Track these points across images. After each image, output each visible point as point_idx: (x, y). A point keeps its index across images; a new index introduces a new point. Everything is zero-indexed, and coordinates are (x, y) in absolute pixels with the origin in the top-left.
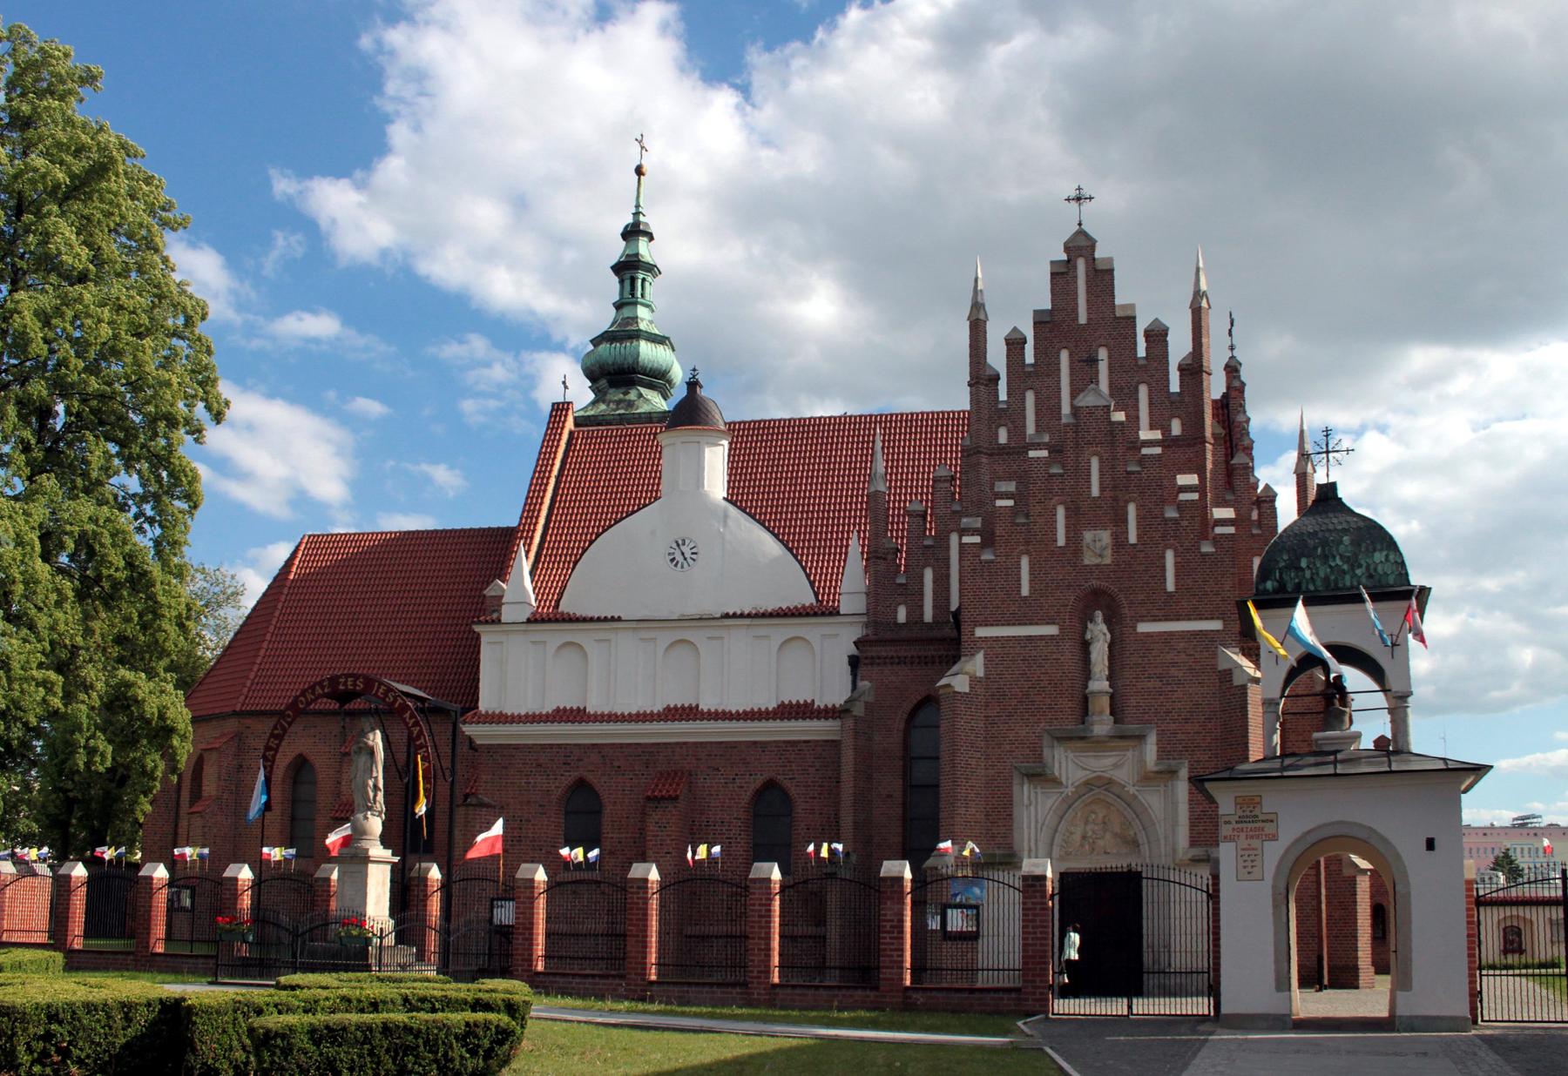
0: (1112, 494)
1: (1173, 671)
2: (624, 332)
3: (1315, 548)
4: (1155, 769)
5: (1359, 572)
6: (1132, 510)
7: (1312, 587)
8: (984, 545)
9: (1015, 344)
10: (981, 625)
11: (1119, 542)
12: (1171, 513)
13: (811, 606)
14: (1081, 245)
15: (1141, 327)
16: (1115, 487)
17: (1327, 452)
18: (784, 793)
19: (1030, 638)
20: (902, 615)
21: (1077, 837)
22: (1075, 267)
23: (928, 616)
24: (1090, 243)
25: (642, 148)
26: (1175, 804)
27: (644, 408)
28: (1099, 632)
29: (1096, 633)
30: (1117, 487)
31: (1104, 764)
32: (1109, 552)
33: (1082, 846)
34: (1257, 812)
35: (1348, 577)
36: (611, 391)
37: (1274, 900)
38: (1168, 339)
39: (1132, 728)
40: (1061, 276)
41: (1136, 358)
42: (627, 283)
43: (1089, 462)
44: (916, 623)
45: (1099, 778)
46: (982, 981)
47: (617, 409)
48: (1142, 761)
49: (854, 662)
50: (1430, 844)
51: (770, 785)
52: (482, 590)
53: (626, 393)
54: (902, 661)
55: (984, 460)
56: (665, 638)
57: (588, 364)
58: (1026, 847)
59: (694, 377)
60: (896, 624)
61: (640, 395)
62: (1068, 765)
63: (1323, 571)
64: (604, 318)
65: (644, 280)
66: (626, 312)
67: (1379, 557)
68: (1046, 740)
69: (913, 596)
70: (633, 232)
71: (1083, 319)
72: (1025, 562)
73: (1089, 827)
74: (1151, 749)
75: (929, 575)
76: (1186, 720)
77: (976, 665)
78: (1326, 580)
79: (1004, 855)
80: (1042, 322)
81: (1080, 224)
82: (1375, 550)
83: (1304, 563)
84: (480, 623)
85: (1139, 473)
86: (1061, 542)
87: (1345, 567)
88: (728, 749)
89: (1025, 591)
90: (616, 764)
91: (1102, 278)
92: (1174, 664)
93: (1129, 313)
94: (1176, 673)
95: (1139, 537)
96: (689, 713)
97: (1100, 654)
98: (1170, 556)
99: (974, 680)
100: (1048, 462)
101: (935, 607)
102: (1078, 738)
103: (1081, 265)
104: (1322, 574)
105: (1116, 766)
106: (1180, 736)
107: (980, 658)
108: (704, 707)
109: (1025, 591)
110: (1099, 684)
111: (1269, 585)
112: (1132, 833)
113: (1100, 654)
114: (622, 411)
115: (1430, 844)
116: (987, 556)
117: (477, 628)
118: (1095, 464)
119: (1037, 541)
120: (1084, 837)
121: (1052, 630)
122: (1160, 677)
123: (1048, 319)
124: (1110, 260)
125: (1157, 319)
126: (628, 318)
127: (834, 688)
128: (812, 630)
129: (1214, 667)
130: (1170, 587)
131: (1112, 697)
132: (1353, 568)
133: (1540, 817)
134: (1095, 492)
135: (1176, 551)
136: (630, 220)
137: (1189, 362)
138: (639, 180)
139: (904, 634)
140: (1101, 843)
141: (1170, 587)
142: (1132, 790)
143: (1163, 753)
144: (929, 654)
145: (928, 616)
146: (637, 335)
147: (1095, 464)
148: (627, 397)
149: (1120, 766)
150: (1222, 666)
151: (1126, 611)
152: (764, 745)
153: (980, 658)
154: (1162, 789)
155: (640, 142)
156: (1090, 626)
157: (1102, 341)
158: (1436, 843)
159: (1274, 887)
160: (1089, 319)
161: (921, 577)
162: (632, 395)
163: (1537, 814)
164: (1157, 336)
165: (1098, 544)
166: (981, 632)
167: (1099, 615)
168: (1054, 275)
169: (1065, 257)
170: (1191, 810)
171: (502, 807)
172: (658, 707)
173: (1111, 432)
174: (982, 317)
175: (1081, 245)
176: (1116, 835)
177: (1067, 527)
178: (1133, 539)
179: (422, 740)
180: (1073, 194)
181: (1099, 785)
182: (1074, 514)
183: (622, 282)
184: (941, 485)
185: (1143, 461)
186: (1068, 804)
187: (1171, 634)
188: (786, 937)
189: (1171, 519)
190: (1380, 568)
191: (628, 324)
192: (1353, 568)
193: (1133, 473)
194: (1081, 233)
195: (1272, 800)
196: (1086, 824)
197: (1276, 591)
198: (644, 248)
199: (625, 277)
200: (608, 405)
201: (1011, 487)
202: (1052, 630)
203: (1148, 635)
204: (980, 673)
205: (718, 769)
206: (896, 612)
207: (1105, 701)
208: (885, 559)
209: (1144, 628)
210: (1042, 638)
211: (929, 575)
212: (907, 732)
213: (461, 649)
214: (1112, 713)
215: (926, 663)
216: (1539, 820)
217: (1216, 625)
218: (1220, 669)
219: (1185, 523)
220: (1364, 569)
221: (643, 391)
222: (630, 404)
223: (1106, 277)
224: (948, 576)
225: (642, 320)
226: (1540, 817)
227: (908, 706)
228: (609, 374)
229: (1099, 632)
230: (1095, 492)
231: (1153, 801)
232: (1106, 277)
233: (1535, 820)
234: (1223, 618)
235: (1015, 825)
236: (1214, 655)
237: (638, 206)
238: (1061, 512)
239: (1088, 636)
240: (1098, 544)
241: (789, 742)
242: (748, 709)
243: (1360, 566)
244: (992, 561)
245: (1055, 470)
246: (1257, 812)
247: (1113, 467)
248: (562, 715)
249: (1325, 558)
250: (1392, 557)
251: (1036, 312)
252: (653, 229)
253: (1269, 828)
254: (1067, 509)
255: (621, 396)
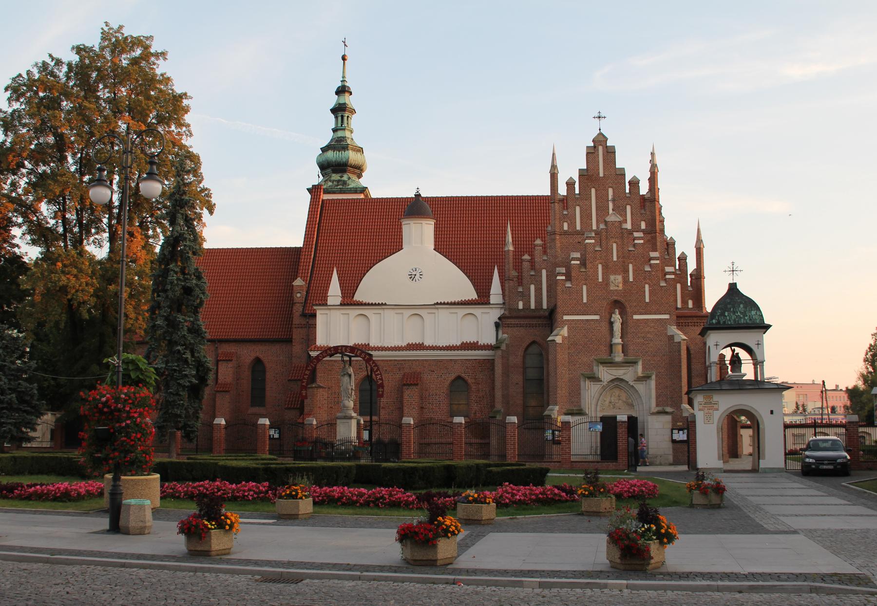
0: (622, 260)
1: (649, 335)
2: (338, 144)
3: (730, 309)
4: (642, 375)
5: (746, 318)
6: (631, 266)
7: (729, 323)
8: (566, 280)
9: (570, 184)
10: (566, 315)
11: (625, 280)
12: (647, 269)
13: (477, 300)
14: (600, 140)
15: (628, 178)
16: (624, 257)
17: (733, 271)
18: (465, 381)
19: (587, 320)
20: (521, 305)
21: (607, 402)
22: (598, 150)
23: (533, 306)
24: (605, 139)
25: (345, 45)
26: (650, 389)
27: (352, 185)
28: (617, 318)
29: (616, 318)
30: (625, 257)
31: (619, 373)
32: (621, 285)
33: (609, 406)
34: (711, 401)
35: (742, 320)
36: (334, 175)
37: (717, 430)
38: (640, 185)
39: (631, 358)
40: (591, 153)
41: (626, 193)
42: (340, 118)
43: (612, 246)
44: (527, 309)
45: (617, 378)
46: (573, 459)
47: (338, 185)
48: (636, 372)
49: (497, 325)
50: (772, 412)
51: (459, 378)
52: (291, 283)
53: (341, 177)
54: (521, 326)
55: (558, 237)
56: (408, 313)
57: (321, 160)
58: (587, 407)
59: (418, 192)
60: (518, 309)
61: (349, 178)
62: (606, 374)
63: (734, 317)
64: (327, 137)
65: (348, 117)
66: (340, 134)
67: (753, 313)
68: (595, 363)
69: (526, 297)
70: (342, 90)
71: (601, 175)
72: (585, 287)
73: (612, 398)
74: (640, 367)
75: (532, 287)
76: (654, 356)
77: (565, 331)
78: (735, 320)
79: (577, 410)
80: (582, 174)
81: (600, 130)
82: (752, 310)
83: (726, 314)
84: (317, 305)
85: (634, 251)
86: (600, 280)
87: (742, 316)
88: (438, 362)
89: (585, 301)
90: (385, 369)
91: (610, 153)
92: (649, 332)
93: (622, 172)
94: (650, 336)
95: (634, 279)
96: (420, 347)
97: (617, 327)
98: (647, 286)
99: (564, 338)
100: (594, 245)
101: (535, 302)
102: (609, 363)
103: (600, 148)
104: (733, 318)
105: (624, 374)
106: (652, 362)
107: (566, 328)
108: (427, 344)
109: (585, 301)
110: (617, 340)
111: (714, 321)
112: (630, 401)
113: (617, 327)
114: (341, 187)
115: (772, 412)
116: (568, 285)
117: (315, 308)
118: (615, 245)
119: (590, 280)
120: (610, 402)
121: (597, 317)
122: (643, 338)
123: (586, 174)
124: (613, 147)
125: (614, 146)
126: (341, 137)
127: (488, 337)
128: (478, 311)
129: (666, 334)
130: (647, 300)
131: (623, 346)
132: (744, 316)
133: (778, 378)
134: (615, 259)
135: (649, 285)
136: (340, 84)
137: (695, 273)
138: (344, 63)
139: (522, 313)
140: (618, 405)
141: (647, 300)
142: (632, 384)
143: (644, 368)
144: (534, 323)
145: (533, 306)
146: (345, 148)
147: (615, 245)
148: (343, 179)
149: (627, 374)
150: (669, 334)
151: (628, 310)
152: (456, 361)
153: (566, 328)
154: (644, 382)
155: (344, 42)
156: (613, 315)
157: (610, 185)
158: (774, 412)
159: (718, 426)
160: (604, 175)
161: (529, 289)
162: (345, 178)
163: (776, 376)
164: (635, 183)
165: (617, 281)
166: (566, 317)
167: (617, 311)
168: (588, 154)
169: (592, 145)
170: (657, 392)
171: (329, 388)
172: (404, 344)
173: (622, 233)
174: (556, 172)
175: (600, 140)
176: (624, 402)
177: (603, 273)
178: (631, 279)
179: (379, 372)
180: (597, 115)
181: (618, 382)
182: (606, 268)
183: (336, 117)
184: (538, 248)
185: (634, 245)
186: (604, 388)
187: (648, 320)
188: (467, 444)
189: (647, 271)
190: (754, 317)
191: (341, 141)
192: (744, 316)
193: (631, 251)
194: (601, 134)
195: (717, 398)
196: (611, 397)
197: (716, 324)
198: (351, 101)
199: (338, 115)
200: (333, 183)
201: (578, 255)
202: (597, 317)
203: (638, 320)
204: (566, 335)
205: (433, 371)
206: (518, 304)
207: (620, 347)
208: (513, 280)
209: (636, 317)
210: (592, 320)
211: (532, 287)
212: (524, 357)
213: (269, 309)
214: (623, 352)
215: (533, 327)
216: (777, 380)
217: (667, 317)
218: (669, 334)
219: (653, 273)
220: (748, 317)
221: (351, 175)
222: (345, 183)
223: (612, 155)
224: (541, 289)
225: (348, 138)
226: (778, 378)
227: (525, 345)
228: (333, 166)
229: (617, 318)
230: (615, 259)
231: (640, 387)
232: (612, 155)
233: (774, 380)
234: (669, 314)
235: (582, 398)
236: (666, 329)
237: (343, 77)
238: (600, 267)
239: (612, 320)
240: (617, 281)
241: (467, 360)
242: (448, 345)
243: (747, 316)
244: (570, 287)
245: (598, 249)
246: (711, 401)
247: (623, 248)
248: (411, 347)
249: (734, 312)
250: (758, 313)
251: (580, 170)
252: (352, 90)
253: (716, 406)
254: (603, 266)
255: (339, 178)
